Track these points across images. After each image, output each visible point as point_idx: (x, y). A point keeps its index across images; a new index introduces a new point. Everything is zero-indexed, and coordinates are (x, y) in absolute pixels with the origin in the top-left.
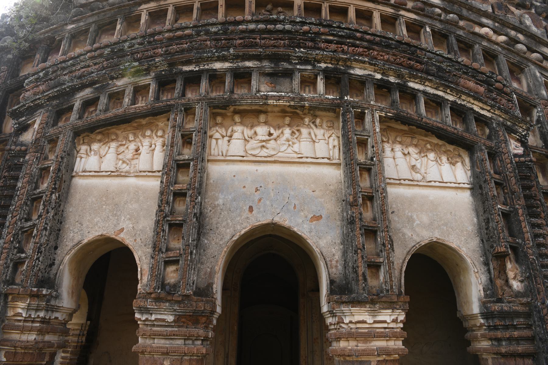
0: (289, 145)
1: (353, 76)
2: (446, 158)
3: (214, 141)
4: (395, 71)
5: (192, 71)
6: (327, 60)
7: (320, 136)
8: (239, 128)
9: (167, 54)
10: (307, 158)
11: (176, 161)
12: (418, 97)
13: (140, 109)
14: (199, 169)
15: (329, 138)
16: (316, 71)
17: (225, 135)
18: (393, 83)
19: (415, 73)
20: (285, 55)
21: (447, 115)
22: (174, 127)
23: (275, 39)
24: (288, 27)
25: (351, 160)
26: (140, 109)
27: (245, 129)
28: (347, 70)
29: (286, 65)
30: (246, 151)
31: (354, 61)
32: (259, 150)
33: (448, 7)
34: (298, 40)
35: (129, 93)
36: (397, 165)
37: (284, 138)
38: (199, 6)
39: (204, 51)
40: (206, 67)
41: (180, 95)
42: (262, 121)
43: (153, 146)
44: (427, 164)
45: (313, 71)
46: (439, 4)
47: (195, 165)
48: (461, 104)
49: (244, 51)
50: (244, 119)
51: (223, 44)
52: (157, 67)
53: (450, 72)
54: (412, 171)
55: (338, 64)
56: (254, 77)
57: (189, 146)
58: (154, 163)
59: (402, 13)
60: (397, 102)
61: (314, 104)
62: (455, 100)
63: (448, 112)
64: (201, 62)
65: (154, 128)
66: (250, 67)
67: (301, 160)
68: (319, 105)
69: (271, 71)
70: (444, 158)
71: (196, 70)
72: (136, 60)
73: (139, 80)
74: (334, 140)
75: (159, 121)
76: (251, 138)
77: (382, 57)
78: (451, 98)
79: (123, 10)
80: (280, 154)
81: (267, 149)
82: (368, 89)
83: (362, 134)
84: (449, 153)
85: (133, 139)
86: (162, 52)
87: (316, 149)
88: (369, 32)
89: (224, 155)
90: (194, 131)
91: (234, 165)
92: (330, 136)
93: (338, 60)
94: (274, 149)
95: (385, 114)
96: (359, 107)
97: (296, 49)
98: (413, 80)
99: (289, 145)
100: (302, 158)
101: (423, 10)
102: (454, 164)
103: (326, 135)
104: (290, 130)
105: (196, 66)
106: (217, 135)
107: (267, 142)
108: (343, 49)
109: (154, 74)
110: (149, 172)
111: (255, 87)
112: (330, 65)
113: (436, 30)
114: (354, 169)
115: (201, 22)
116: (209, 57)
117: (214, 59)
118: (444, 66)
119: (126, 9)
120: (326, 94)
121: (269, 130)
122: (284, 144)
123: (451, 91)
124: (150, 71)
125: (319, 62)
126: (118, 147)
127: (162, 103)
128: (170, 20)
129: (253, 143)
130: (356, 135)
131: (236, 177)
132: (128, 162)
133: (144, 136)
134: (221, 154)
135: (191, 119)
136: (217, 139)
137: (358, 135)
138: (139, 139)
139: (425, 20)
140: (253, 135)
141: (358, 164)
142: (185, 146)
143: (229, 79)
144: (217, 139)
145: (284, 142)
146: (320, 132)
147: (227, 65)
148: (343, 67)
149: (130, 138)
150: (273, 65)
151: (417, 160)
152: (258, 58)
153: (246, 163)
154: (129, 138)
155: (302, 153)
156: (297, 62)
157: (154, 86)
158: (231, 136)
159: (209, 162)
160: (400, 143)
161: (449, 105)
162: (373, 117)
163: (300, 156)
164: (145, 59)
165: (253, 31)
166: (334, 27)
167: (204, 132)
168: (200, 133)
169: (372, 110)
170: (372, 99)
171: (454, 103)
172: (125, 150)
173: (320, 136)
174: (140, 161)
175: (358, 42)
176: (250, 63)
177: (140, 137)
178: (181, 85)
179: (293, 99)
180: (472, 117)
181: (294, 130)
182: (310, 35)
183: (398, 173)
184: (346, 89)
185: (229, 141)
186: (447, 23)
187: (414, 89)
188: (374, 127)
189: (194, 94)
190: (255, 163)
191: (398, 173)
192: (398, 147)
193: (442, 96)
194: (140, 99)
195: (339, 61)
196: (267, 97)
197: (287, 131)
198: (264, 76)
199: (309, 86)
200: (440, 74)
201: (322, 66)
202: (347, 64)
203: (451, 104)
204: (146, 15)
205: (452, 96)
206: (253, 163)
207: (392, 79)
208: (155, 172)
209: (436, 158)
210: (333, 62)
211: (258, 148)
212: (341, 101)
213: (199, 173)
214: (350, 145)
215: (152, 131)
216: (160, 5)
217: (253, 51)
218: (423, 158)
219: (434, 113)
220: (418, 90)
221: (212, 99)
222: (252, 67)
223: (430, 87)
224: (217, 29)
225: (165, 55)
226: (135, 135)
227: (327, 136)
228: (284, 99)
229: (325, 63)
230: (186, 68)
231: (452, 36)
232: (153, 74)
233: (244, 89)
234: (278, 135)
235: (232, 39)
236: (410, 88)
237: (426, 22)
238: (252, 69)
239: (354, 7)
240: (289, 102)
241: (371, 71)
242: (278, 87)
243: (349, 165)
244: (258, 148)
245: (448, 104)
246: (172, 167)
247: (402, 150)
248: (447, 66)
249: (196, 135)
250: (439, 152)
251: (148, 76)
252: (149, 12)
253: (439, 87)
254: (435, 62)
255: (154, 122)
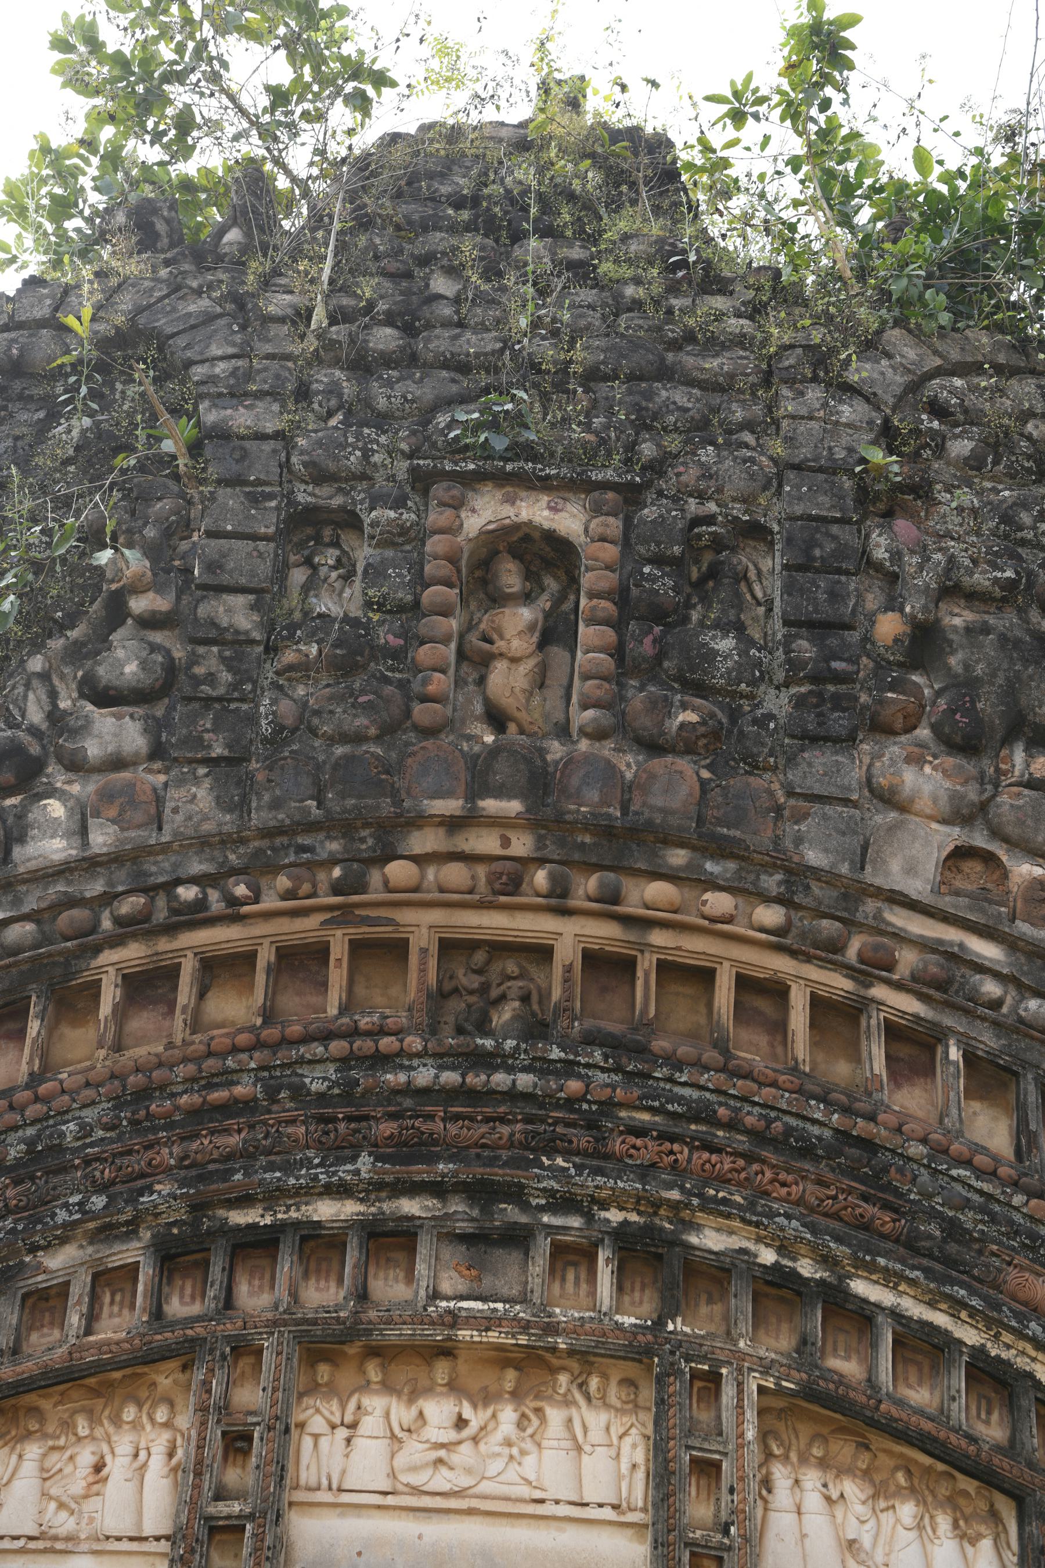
0: (511, 1457)
1: (697, 1253)
2: (949, 1519)
3: (307, 1442)
4: (814, 1248)
5: (254, 1226)
6: (626, 1202)
7: (596, 1435)
8: (375, 1403)
9: (187, 1167)
10: (557, 1502)
11: (209, 1518)
12: (876, 1326)
13: (111, 1352)
14: (269, 1548)
15: (621, 1438)
16: (595, 1233)
17: (339, 1422)
18: (807, 1279)
19: (868, 1258)
20: (510, 1184)
21: (953, 1392)
22: (203, 1409)
23: (487, 1120)
24: (525, 1081)
25: (669, 1531)
26: (111, 1352)
27: (394, 1401)
28: (682, 1233)
29: (511, 1213)
30: (393, 1475)
31: (701, 1211)
32: (430, 1471)
33: (1024, 973)
34: (550, 1125)
35: (81, 1296)
36: (804, 1536)
37: (498, 1436)
38: (273, 959)
39: (288, 1161)
40: (294, 1214)
41: (221, 1305)
42: (440, 1381)
43: (143, 1454)
44: (892, 1537)
45: (586, 1233)
46: (999, 962)
47: (257, 1535)
48: (998, 1356)
49: (398, 1172)
50: (393, 1366)
51: (340, 1139)
52: (157, 1215)
53: (984, 1239)
54: (848, 1555)
55: (656, 1214)
56: (424, 1251)
57: (240, 1459)
58: (145, 1509)
59: (879, 992)
60: (813, 1344)
61: (584, 1341)
62: (983, 1345)
63: (959, 1380)
64: (278, 1198)
65: (143, 1393)
66: (413, 1218)
67: (540, 1510)
68: (596, 1347)
69: (471, 1230)
70: (944, 1522)
71: (266, 1225)
72: (102, 1188)
73: (108, 1253)
74: (634, 1446)
75: (158, 1372)
76: (409, 1431)
77: (784, 1191)
78: (970, 1336)
79: (46, 965)
80: (485, 1483)
81: (452, 1469)
82: (736, 1296)
83: (706, 1446)
84: (962, 1502)
85: (87, 1432)
86: (172, 1162)
87: (583, 1472)
88: (756, 1099)
89: (335, 1486)
90: (259, 1424)
91: (359, 1516)
92: (625, 1434)
93: (657, 1204)
94: (469, 1471)
95: (776, 1384)
96: (704, 1359)
97: (544, 1159)
98: (865, 1274)
99: (511, 1457)
100: (541, 1501)
101: (943, 986)
102: (973, 1541)
103: (613, 1430)
104: (515, 1411)
105: (264, 1209)
106: (317, 1424)
107: (452, 1448)
108: (676, 1161)
109: (149, 1234)
110: (131, 1539)
111: (425, 1284)
112: (634, 1217)
113: (980, 1053)
114: (674, 1558)
115: (279, 1055)
116: (301, 1188)
117: (317, 1191)
118: (967, 1218)
119: (54, 964)
120: (617, 1313)
121: (457, 1409)
122: (499, 1455)
123: (970, 1316)
124: (138, 1226)
125: (604, 1206)
126: (44, 1455)
127: (173, 1332)
128: (185, 1008)
129: (414, 1451)
130: (688, 1447)
131: (363, 1558)
132: (73, 1505)
133: (117, 1421)
134: (325, 1482)
135: (248, 1370)
136: (316, 1437)
137: (694, 1448)
138: (101, 1429)
139: (948, 1020)
140: (416, 1420)
141: (686, 1545)
142: (231, 1459)
143: (356, 1253)
144: (316, 1437)
145: (498, 1449)
146: (596, 1419)
147: (350, 1209)
148: (671, 1223)
149: (80, 1429)
150: (475, 1213)
151: (863, 1522)
152: (437, 1189)
153: (391, 1512)
154: (75, 1427)
155: (546, 1484)
156: (543, 1202)
157: (151, 1272)
158: (353, 1426)
159: (294, 1508)
160: (823, 1464)
161: (965, 1358)
162: (740, 1391)
163: (538, 1494)
164: (124, 1182)
165: (424, 1093)
166: (658, 1079)
167: (283, 1427)
168: (272, 1433)
169: (740, 1370)
170: (744, 1331)
171: (978, 1352)
172: (66, 1465)
173: (596, 1435)
174: (107, 1504)
175: (720, 1133)
176: (413, 1202)
177: (106, 1422)
178: (224, 1269)
179: (525, 1327)
180: (1027, 1402)
181: (527, 1411)
182: (585, 1106)
183: (805, 1560)
184: (673, 1296)
185: (348, 1441)
186: (1018, 1033)
187: (865, 1301)
188: (740, 1424)
189: (257, 1282)
190: (418, 1514)
191: (805, 1560)
192: (812, 1478)
193: (946, 1330)
194: (107, 1299)
195: (659, 1207)
196: (453, 1319)
197: (508, 1415)
198: (451, 1242)
199: (575, 1264)
200: (952, 1248)
201: (612, 1219)
202: (682, 1215)
203: (971, 1356)
204: (116, 986)
205: (974, 1332)
206: (411, 1514)
207: (806, 1268)
208: (145, 1539)
209: (922, 1518)
210: (642, 1208)
211: (424, 1466)
212: (655, 1337)
213: (268, 1558)
214: (670, 1483)
215: (140, 1406)
216: (157, 954)
217: (420, 1172)
218: (885, 1514)
219: (926, 1369)
220: (877, 1306)
221: (306, 1321)
222: (420, 1218)
223: (914, 1297)
224: (326, 1084)
225: (180, 1167)
226: (94, 1419)
227: (616, 1431)
228: (500, 1326)
229: (621, 1209)
230: (239, 1218)
231: (1030, 1076)
232: (146, 1235)
233: (395, 1267)
234: (482, 1424)
235: (366, 1118)
236: (856, 1296)
237: (949, 1028)
238: (418, 1223)
239: (734, 970)
240: (514, 1337)
241: (749, 1239)
242: (488, 1283)
243: (663, 1545)
244: (424, 1466)
245: (961, 1353)
246: (197, 1540)
247: (825, 1485)
248: (976, 1222)
249: (262, 1439)
250: (930, 1499)
251: (132, 1239)
252: (124, 976)
253: (937, 1302)
254: (942, 1205)
255: (146, 1374)
